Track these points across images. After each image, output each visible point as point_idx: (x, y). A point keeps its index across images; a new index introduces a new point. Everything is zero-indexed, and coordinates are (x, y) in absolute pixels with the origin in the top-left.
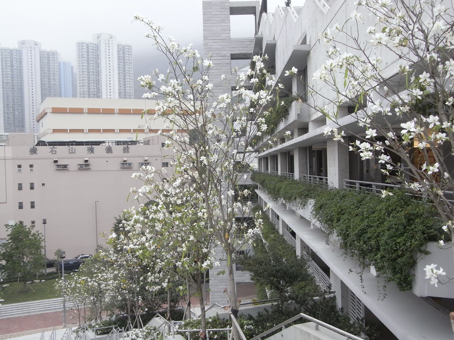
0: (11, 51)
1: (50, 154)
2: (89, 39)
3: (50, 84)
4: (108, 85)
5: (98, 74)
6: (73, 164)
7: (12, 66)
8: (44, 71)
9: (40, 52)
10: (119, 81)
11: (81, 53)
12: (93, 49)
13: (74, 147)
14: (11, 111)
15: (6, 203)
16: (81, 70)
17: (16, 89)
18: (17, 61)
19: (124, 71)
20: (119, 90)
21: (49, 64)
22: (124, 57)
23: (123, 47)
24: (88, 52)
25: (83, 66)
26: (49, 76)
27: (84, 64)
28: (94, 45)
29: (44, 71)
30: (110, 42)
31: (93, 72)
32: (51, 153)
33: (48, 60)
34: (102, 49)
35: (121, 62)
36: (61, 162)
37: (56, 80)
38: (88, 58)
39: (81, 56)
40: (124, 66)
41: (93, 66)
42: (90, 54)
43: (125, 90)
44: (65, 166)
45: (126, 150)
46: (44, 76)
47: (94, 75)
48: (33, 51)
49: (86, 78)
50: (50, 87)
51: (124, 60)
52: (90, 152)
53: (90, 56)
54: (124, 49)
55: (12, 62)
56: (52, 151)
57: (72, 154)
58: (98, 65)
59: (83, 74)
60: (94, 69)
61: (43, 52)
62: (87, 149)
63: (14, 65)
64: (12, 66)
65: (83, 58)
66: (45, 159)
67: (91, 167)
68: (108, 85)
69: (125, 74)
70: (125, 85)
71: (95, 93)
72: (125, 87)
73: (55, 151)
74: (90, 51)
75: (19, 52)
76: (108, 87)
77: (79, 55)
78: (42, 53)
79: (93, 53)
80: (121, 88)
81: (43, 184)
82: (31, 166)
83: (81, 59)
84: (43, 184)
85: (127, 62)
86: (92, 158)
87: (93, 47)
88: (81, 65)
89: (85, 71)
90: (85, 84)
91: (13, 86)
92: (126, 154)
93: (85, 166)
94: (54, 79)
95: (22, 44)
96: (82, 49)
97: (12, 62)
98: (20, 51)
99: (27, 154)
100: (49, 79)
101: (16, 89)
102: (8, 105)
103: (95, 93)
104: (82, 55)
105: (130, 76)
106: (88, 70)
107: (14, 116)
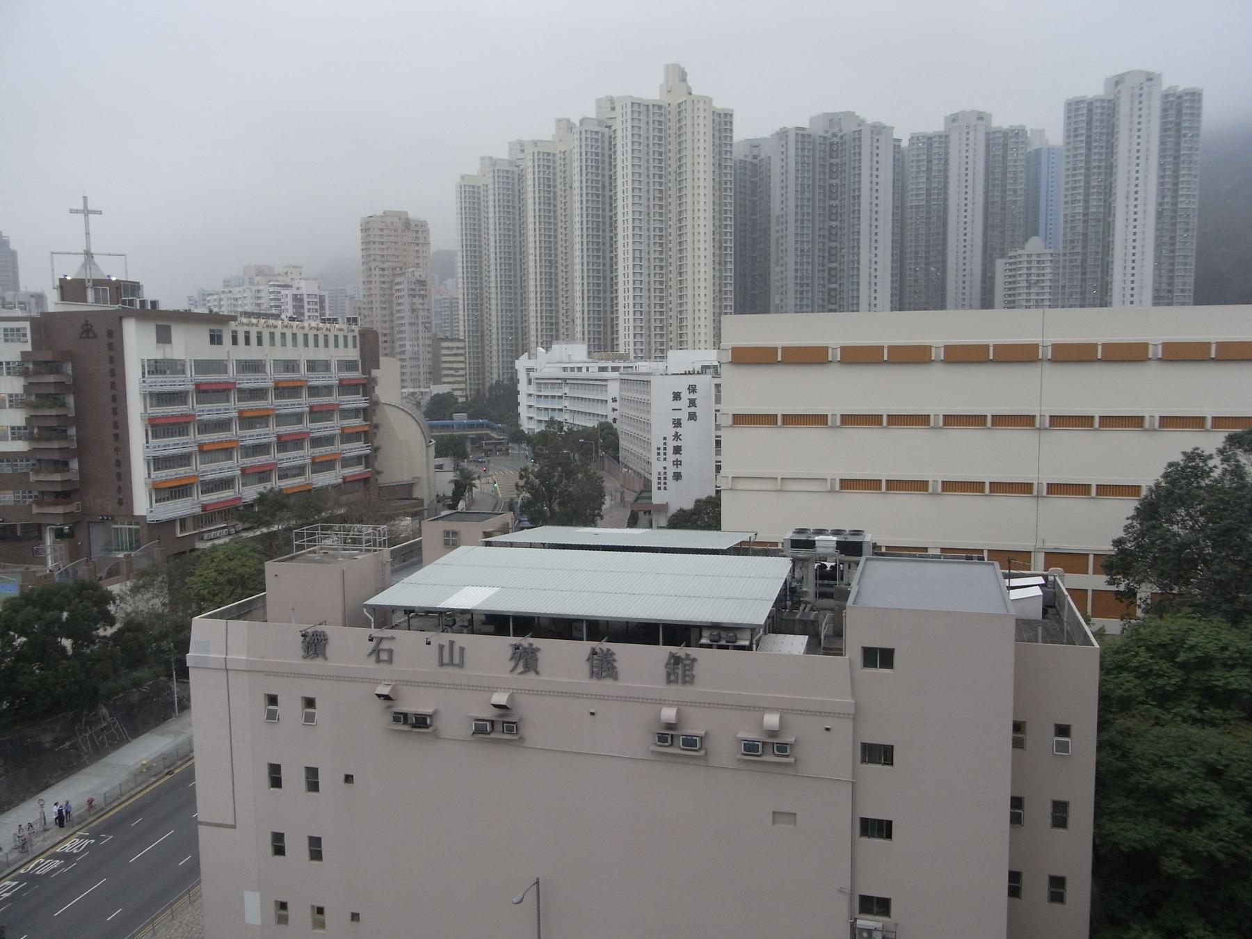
0: (930, 138)
1: (371, 663)
2: (1094, 89)
3: (1004, 203)
4: (1132, 196)
5: (1110, 170)
6: (458, 709)
7: (929, 170)
8: (993, 174)
9: (987, 134)
10: (1162, 184)
11: (1073, 126)
12: (1102, 114)
13: (463, 639)
14: (922, 265)
15: (234, 827)
16: (1070, 166)
17: (934, 219)
18: (940, 160)
19: (1176, 158)
20: (1160, 204)
21: (1004, 157)
22: (1179, 124)
23: (1179, 97)
24: (1089, 122)
25: (1075, 156)
26: (1004, 185)
27: (1080, 151)
28: (1105, 104)
29: (993, 174)
30: (1145, 90)
31: (1099, 167)
32: (373, 657)
33: (1003, 147)
34: (1124, 110)
35: (1169, 136)
36: (413, 704)
37: (1019, 192)
38: (1089, 137)
39: (1071, 133)
40: (1178, 144)
41: (1101, 154)
42: (1094, 123)
43: (1175, 204)
44: (421, 722)
45: (679, 671)
46: (994, 186)
47: (1099, 174)
48: (971, 135)
49: (1082, 184)
50: (1004, 209)
51: (1178, 131)
52: (520, 668)
53: (1094, 131)
54: (1180, 104)
55: (929, 162)
56: (376, 652)
57: (451, 670)
58: (1111, 149)
59: (1074, 175)
60: (1101, 161)
61: (994, 133)
62: (509, 652)
63: (935, 168)
64: (929, 170)
65: (1076, 136)
66: (353, 679)
67: (528, 731)
68: (1132, 196)
69: (1178, 164)
70: (1176, 191)
71: (1101, 216)
72: (1175, 197)
73: (391, 652)
74: (1095, 118)
75: (944, 138)
76: (1131, 200)
77: (1068, 130)
78: (990, 136)
79: (1102, 121)
80: (1166, 200)
81: (349, 779)
82: (310, 703)
83: (1072, 139)
84: (349, 779)
85: (1185, 135)
86: (530, 692)
87: (1103, 108)
88: (1070, 153)
89: (1081, 168)
90: (1078, 197)
91: (928, 212)
92: (677, 691)
93: (501, 726)
94: (1015, 191)
95: (953, 121)
96: (1076, 116)
97: (929, 162)
98: (947, 137)
99: (293, 655)
100: (1004, 192)
101: (934, 219)
102: (917, 253)
103: (1101, 216)
104: (1076, 130)
105: (1190, 169)
106: (1088, 162)
107: (927, 275)
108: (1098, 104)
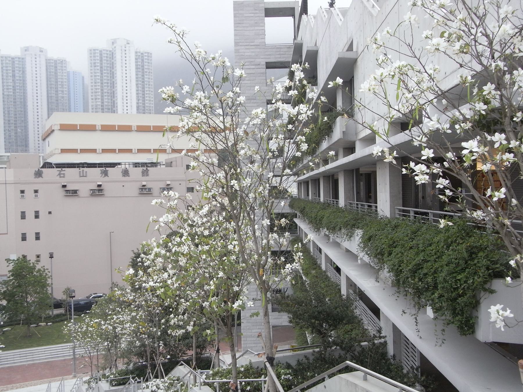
0: (13, 58)
1: (58, 177)
2: (103, 45)
3: (57, 97)
4: (125, 98)
5: (113, 85)
6: (84, 189)
7: (14, 76)
8: (50, 81)
9: (46, 60)
10: (137, 94)
11: (93, 62)
12: (107, 57)
13: (85, 169)
14: (13, 128)
15: (7, 234)
16: (93, 81)
17: (18, 103)
18: (20, 71)
19: (143, 82)
20: (137, 103)
21: (56, 73)
22: (143, 66)
23: (142, 54)
24: (101, 60)
25: (95, 76)
26: (57, 88)
27: (97, 74)
28: (108, 52)
29: (50, 81)
30: (127, 49)
31: (108, 83)
32: (59, 176)
33: (55, 69)
34: (118, 56)
35: (139, 72)
36: (70, 187)
37: (65, 92)
38: (101, 67)
39: (93, 65)
40: (143, 76)
41: (108, 77)
42: (104, 62)
43: (144, 104)
44: (75, 192)
45: (145, 173)
46: (51, 88)
47: (108, 86)
48: (38, 59)
49: (100, 90)
50: (57, 100)
51: (143, 70)
52: (103, 176)
53: (104, 65)
54: (142, 57)
55: (13, 71)
56: (60, 174)
57: (83, 178)
58: (113, 75)
59: (95, 86)
60: (108, 80)
61: (50, 60)
62: (100, 172)
63: (17, 75)
64: (14, 76)
65: (95, 66)
66: (52, 183)
67: (105, 192)
68: (125, 98)
69: (144, 85)
70: (144, 98)
71: (110, 107)
72: (144, 101)
73: (64, 174)
74: (103, 58)
75: (22, 60)
76: (125, 100)
77: (91, 63)
78: (48, 61)
79: (107, 61)
80: (140, 101)
81: (50, 213)
82: (36, 191)
83: (93, 68)
84: (50, 213)
85: (146, 72)
86: (106, 182)
87: (107, 54)
88: (93, 75)
89: (98, 82)
90: (98, 97)
91: (15, 99)
92: (145, 178)
93: (98, 191)
94: (63, 91)
95: (26, 50)
96: (94, 57)
97: (13, 71)
98: (23, 59)
99: (31, 177)
100: (57, 91)
101: (18, 103)
102: (9, 121)
103: (110, 107)
104: (95, 63)
105: (149, 88)
106: (101, 80)
107: (16, 133)
108: (17, 59)
